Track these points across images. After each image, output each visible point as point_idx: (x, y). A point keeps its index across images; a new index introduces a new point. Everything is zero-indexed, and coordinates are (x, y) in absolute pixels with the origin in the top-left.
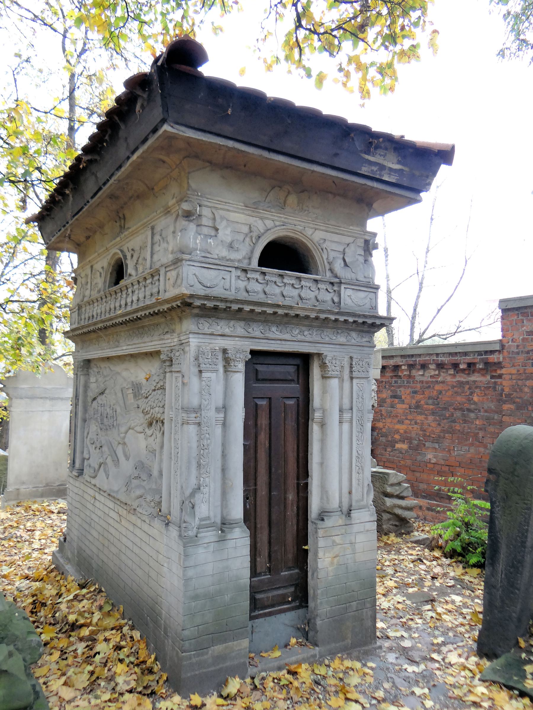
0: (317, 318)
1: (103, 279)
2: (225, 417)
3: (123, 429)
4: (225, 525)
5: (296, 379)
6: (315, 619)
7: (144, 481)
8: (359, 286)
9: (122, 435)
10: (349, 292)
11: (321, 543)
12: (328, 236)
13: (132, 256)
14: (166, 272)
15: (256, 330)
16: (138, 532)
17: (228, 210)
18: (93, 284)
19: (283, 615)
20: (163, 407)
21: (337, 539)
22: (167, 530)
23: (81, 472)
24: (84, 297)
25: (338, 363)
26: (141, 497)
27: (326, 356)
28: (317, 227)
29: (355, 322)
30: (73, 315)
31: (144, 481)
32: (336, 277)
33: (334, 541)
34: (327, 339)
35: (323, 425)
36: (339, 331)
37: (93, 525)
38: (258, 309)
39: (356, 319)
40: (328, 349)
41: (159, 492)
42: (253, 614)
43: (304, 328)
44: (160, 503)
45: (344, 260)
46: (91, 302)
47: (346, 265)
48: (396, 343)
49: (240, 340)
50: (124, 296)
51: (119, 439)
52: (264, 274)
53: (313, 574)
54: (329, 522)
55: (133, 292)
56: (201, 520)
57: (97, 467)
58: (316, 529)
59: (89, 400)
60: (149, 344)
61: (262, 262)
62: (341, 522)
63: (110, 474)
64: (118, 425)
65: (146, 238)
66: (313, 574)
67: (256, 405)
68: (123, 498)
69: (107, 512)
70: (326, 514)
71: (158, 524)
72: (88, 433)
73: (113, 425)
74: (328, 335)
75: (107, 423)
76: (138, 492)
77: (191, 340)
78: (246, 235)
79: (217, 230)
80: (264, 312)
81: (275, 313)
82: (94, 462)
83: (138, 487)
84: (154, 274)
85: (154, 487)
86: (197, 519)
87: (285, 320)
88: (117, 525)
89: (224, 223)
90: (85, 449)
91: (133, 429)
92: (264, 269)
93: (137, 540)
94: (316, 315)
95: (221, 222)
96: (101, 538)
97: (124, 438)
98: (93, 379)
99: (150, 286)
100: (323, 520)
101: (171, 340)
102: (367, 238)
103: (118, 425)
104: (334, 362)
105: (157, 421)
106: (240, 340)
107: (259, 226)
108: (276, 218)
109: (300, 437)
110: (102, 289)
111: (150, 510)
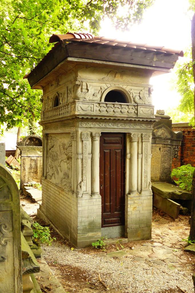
0: (127, 120)
1: (52, 103)
2: (92, 157)
3: (60, 161)
4: (93, 193)
5: (120, 143)
6: (127, 229)
7: (66, 179)
8: (146, 106)
9: (60, 163)
10: (142, 109)
11: (129, 202)
12: (133, 88)
13: (61, 96)
14: (71, 105)
15: (103, 125)
16: (65, 197)
17: (92, 82)
18: (49, 104)
19: (115, 227)
20: (72, 153)
21: (136, 201)
22: (73, 195)
23: (46, 178)
24: (45, 108)
25: (136, 136)
26: (66, 185)
27: (131, 134)
28: (128, 85)
29: (143, 120)
30: (42, 115)
31: (66, 179)
32: (136, 103)
33: (134, 202)
34: (132, 127)
35: (131, 159)
36: (137, 124)
37: (51, 197)
38: (103, 118)
39: (143, 120)
40: (132, 131)
41: (70, 183)
42: (14, 152)
43: (122, 124)
44: (71, 187)
45: (139, 96)
46: (48, 111)
47: (140, 98)
48: (172, 125)
49: (97, 129)
50: (59, 111)
51: (58, 165)
52: (107, 104)
53: (126, 213)
54: (132, 195)
55: (62, 110)
56: (83, 192)
57: (51, 175)
58: (128, 197)
59: (49, 150)
60: (67, 130)
61: (106, 100)
62: (137, 195)
63: (56, 177)
64: (58, 159)
65: (65, 91)
66: (126, 213)
67: (116, 152)
68: (60, 185)
69: (55, 191)
70: (131, 192)
71: (70, 193)
72: (48, 162)
73: (57, 159)
74: (132, 126)
75: (55, 158)
76: (65, 183)
77: (79, 130)
78: (100, 90)
79: (88, 90)
80: (105, 119)
81: (110, 119)
82: (50, 173)
83: (65, 181)
84: (67, 105)
85: (69, 181)
86: (82, 191)
87: (115, 121)
88: (58, 196)
89: (91, 87)
90: (47, 168)
91: (63, 161)
92: (106, 102)
93: (64, 200)
94: (126, 119)
95: (90, 87)
96: (54, 201)
97: (60, 164)
98: (49, 141)
99: (67, 109)
100: (130, 194)
101: (73, 130)
102: (150, 87)
103: (58, 159)
104: (134, 136)
105: (70, 158)
106: (97, 129)
107: (104, 86)
108: (111, 83)
109: (122, 163)
110: (52, 107)
111: (68, 189)
